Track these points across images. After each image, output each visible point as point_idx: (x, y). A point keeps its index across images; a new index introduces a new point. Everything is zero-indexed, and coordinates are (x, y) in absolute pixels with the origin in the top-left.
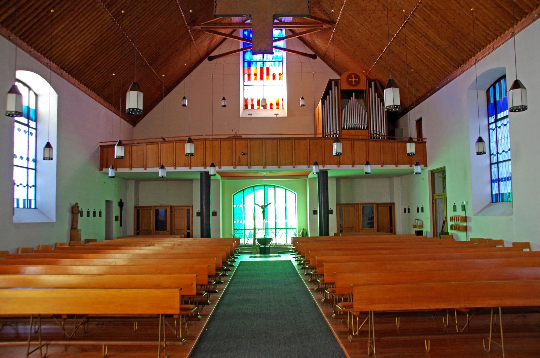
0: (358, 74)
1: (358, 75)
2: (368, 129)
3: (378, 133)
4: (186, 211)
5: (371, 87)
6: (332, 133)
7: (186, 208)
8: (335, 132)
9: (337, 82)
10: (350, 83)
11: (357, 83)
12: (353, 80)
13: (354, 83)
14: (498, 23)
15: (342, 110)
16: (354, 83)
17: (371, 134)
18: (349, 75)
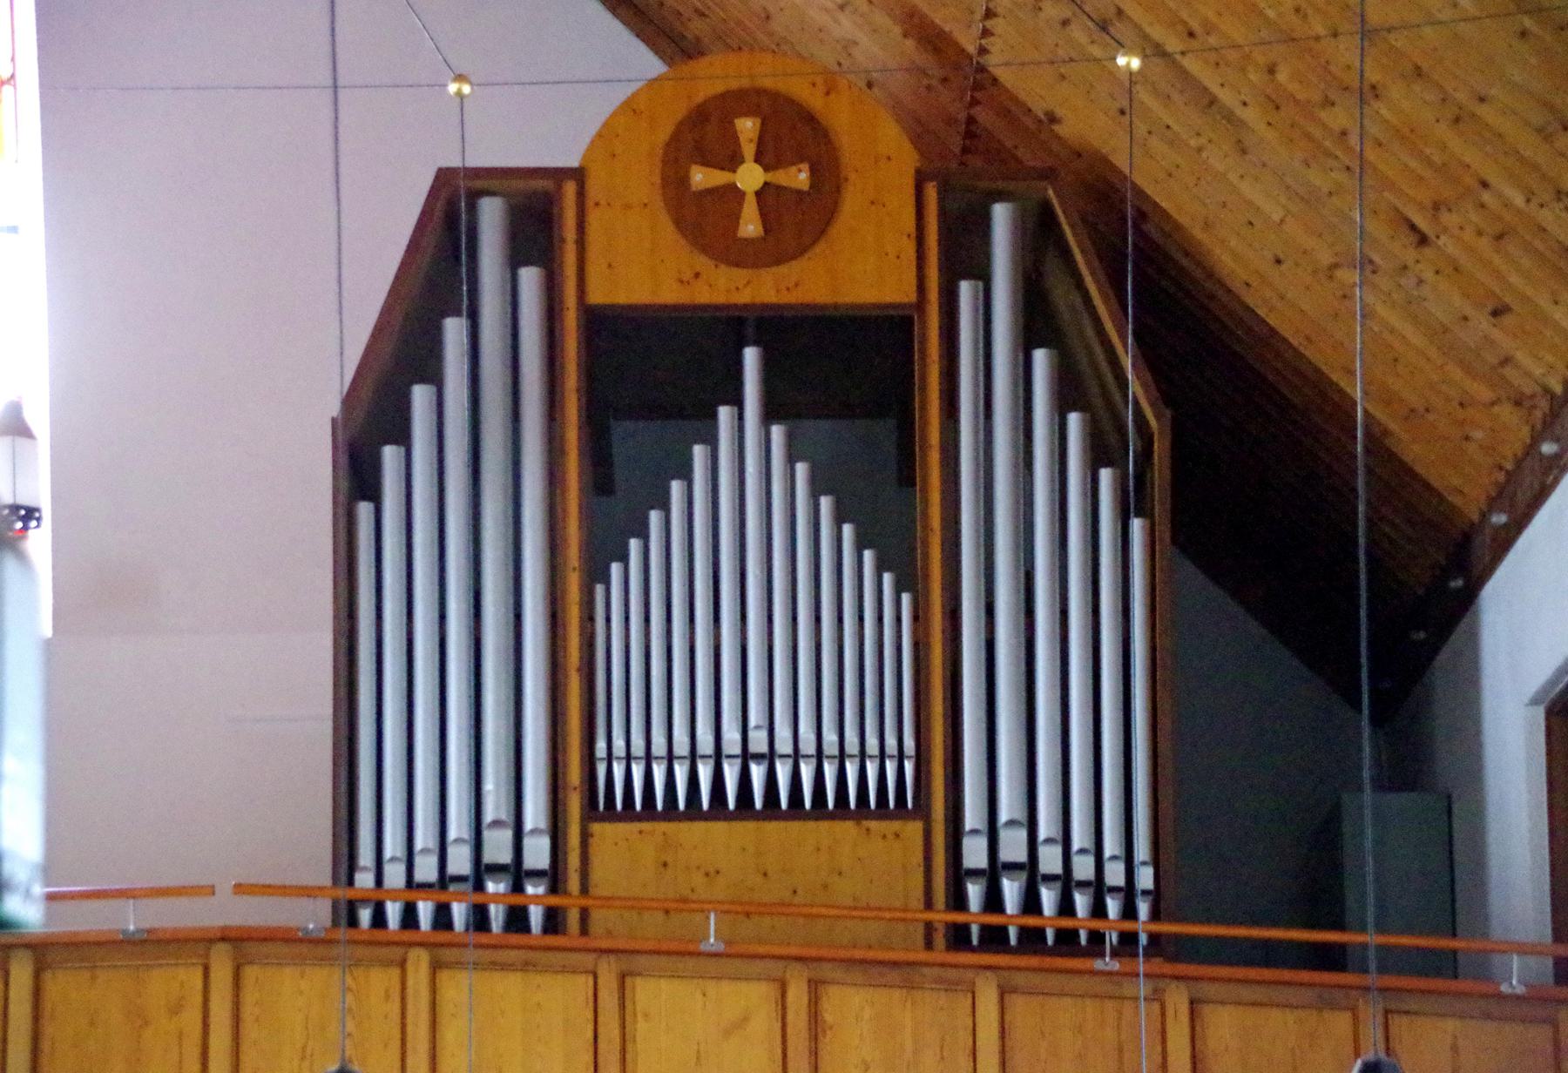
0: (814, 100)
1: (810, 118)
4: (620, 475)
5: (983, 275)
6: (395, 876)
8: (498, 848)
9: (541, 213)
10: (703, 222)
11: (800, 221)
12: (750, 177)
14: (1517, 78)
15: (596, 574)
16: (750, 226)
17: (958, 875)
18: (700, 116)
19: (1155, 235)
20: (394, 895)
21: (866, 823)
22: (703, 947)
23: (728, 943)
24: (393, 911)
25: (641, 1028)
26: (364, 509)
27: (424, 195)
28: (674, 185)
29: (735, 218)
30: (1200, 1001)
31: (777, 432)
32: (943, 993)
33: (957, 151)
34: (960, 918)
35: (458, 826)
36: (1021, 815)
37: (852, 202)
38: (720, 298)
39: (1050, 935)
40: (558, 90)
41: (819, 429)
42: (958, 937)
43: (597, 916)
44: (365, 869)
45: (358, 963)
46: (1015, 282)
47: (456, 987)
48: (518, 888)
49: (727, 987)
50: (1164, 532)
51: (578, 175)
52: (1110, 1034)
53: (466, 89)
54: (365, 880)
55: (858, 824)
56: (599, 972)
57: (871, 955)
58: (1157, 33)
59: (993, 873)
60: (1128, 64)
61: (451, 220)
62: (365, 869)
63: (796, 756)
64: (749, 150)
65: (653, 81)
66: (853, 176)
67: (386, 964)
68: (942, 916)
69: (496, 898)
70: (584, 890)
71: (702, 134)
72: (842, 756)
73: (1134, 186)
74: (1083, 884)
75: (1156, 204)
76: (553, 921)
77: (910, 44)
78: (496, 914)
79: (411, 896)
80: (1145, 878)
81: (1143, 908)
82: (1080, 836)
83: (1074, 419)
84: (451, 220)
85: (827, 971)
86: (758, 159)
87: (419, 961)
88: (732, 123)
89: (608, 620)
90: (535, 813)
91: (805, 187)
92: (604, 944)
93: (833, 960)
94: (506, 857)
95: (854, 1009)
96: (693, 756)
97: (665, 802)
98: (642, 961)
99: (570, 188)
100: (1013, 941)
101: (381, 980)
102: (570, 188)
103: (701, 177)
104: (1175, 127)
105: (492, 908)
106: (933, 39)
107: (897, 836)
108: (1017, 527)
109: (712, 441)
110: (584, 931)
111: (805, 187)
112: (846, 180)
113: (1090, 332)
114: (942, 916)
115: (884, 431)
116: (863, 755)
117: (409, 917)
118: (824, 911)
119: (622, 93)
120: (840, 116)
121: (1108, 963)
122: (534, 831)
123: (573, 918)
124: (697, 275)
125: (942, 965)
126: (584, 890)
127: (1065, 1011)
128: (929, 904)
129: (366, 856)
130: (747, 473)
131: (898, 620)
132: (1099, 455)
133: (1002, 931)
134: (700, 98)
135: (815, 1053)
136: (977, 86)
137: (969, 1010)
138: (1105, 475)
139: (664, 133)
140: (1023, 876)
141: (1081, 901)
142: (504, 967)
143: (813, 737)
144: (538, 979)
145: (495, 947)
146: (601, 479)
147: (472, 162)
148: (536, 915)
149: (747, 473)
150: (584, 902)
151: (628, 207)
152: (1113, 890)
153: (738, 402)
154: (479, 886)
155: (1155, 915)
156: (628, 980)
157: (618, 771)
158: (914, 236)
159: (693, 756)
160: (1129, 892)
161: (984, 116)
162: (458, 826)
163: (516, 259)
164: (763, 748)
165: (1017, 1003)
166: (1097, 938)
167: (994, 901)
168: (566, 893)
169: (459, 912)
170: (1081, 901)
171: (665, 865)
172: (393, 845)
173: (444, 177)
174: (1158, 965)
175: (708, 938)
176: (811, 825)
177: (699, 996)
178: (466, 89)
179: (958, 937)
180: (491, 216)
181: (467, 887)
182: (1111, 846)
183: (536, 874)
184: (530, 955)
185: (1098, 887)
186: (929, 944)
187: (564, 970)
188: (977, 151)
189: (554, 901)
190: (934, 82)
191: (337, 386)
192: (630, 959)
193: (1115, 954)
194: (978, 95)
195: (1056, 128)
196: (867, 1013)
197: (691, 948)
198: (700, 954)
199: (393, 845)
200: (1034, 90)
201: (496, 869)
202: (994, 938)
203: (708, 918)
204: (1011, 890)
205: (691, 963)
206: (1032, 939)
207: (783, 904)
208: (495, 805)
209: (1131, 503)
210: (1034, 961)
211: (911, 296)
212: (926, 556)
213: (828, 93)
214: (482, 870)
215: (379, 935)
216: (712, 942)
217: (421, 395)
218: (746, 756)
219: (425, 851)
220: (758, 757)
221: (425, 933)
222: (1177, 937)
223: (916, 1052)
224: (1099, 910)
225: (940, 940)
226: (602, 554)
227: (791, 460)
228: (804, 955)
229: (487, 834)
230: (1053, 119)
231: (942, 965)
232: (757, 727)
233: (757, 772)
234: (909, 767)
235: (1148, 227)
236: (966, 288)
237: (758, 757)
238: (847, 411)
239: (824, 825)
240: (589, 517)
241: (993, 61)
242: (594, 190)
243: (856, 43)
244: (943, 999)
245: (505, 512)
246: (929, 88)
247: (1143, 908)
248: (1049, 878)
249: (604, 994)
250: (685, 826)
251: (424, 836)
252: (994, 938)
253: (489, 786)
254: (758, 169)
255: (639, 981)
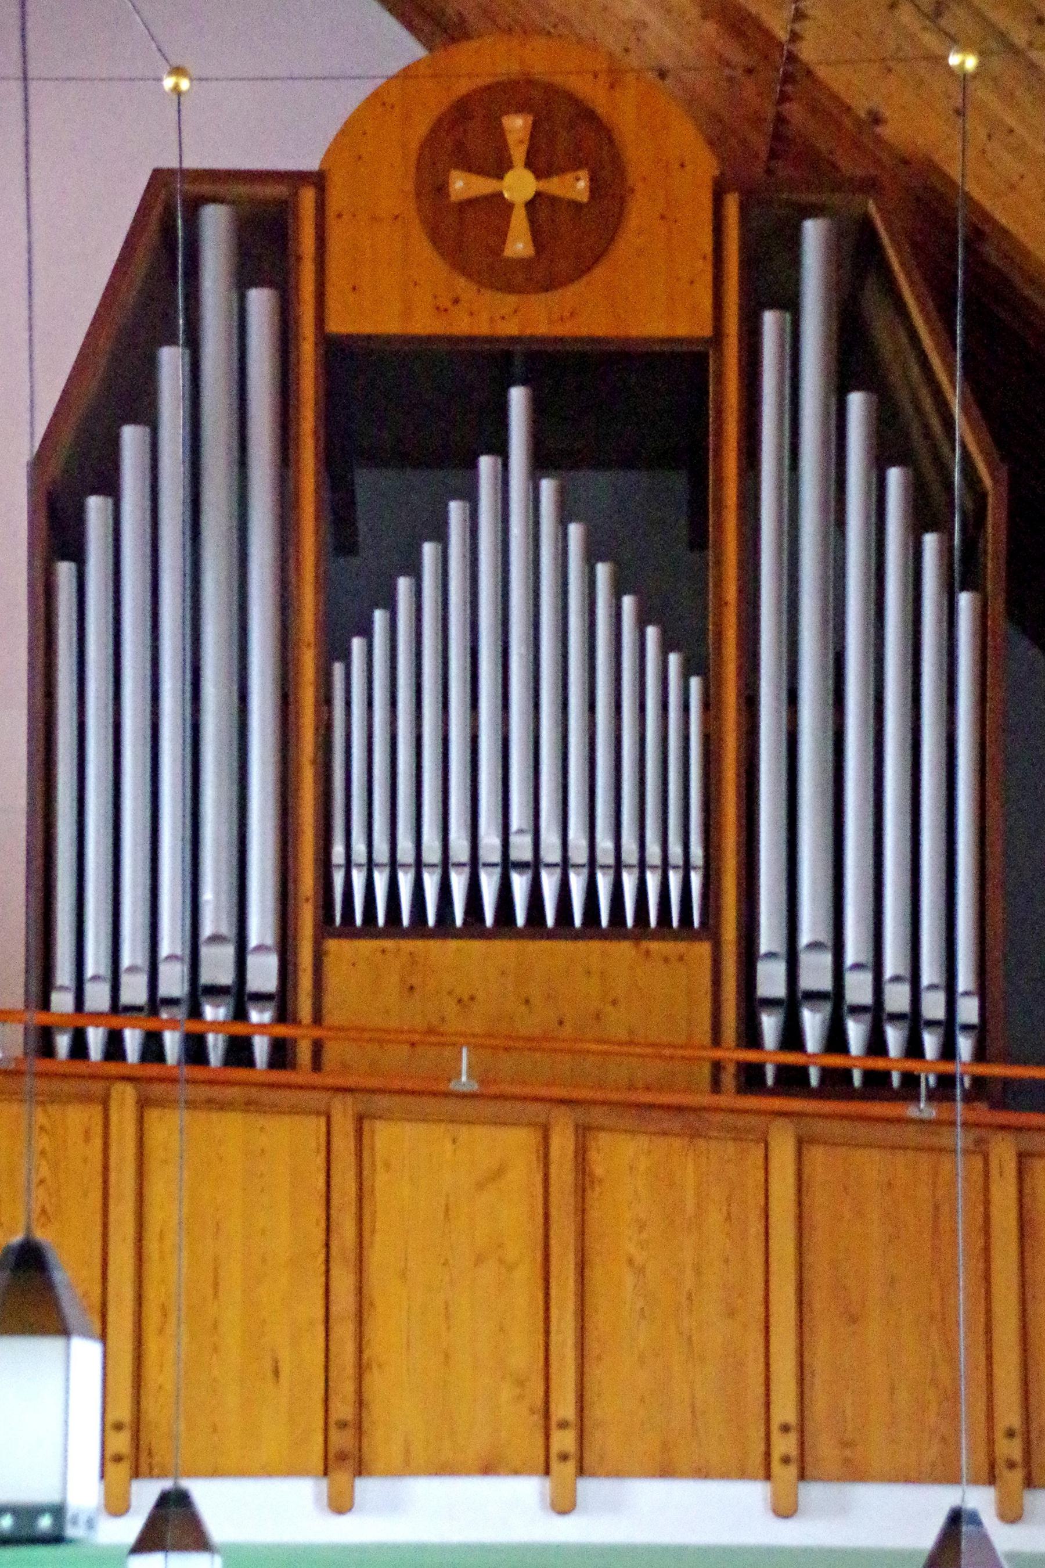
0: (593, 92)
1: (586, 115)
2: (711, 929)
3: (858, 989)
5: (790, 303)
6: (98, 997)
7: (110, 1432)
8: (217, 968)
9: (273, 224)
10: (463, 236)
11: (574, 241)
12: (519, 185)
13: (577, 186)
17: (751, 1005)
18: (460, 112)
19: (994, 259)
20: (96, 1017)
21: (645, 944)
22: (453, 1086)
23: (482, 1082)
24: (96, 1038)
25: (380, 1180)
26: (65, 570)
27: (142, 192)
28: (432, 190)
29: (502, 234)
30: (1031, 1155)
31: (547, 487)
32: (730, 1143)
33: (764, 155)
34: (751, 1056)
35: (171, 940)
36: (825, 936)
37: (640, 213)
38: (482, 328)
39: (814, 1077)
40: (296, 81)
41: (600, 484)
42: (751, 1078)
43: (332, 1052)
44: (62, 988)
45: (54, 1098)
46: (828, 309)
47: (166, 1128)
48: (240, 1014)
49: (480, 1132)
50: (998, 606)
51: (318, 180)
52: (924, 1192)
53: (185, 84)
54: (62, 1002)
55: (637, 945)
56: (333, 1112)
57: (647, 1098)
58: (1001, 18)
59: (791, 1005)
60: (963, 63)
61: (168, 230)
62: (62, 988)
63: (565, 865)
64: (518, 153)
65: (407, 74)
66: (640, 186)
67: (85, 1099)
68: (733, 1054)
69: (261, 1027)
70: (318, 1018)
71: (463, 133)
72: (618, 866)
73: (968, 198)
74: (895, 1017)
75: (995, 223)
76: (281, 1054)
77: (710, 28)
78: (215, 1045)
79: (116, 1022)
80: (968, 1010)
81: (965, 1045)
82: (893, 963)
83: (895, 476)
84: (168, 230)
85: (597, 1115)
86: (529, 164)
87: (124, 1096)
88: (498, 119)
89: (348, 704)
90: (261, 927)
91: (584, 198)
92: (340, 1082)
93: (603, 1103)
94: (226, 977)
95: (625, 1157)
96: (445, 864)
97: (412, 912)
98: (384, 1102)
99: (308, 196)
100: (770, 1081)
101: (79, 1117)
102: (308, 196)
103: (462, 185)
104: (1020, 130)
105: (211, 1038)
106: (740, 26)
107: (681, 958)
108: (906, 563)
109: (471, 497)
110: (317, 1064)
111: (584, 198)
112: (632, 191)
113: (915, 371)
114: (733, 1054)
115: (678, 481)
116: (643, 865)
117: (114, 1047)
118: (594, 1047)
119: (367, 89)
120: (623, 112)
121: (924, 1109)
122: (260, 948)
123: (304, 1053)
124: (456, 301)
125: (732, 1111)
126: (318, 1018)
127: (871, 1165)
128: (716, 1040)
129: (64, 974)
130: (513, 529)
131: (686, 708)
132: (924, 516)
133: (885, 1076)
134: (463, 87)
135: (582, 1212)
136: (788, 78)
137: (760, 1162)
138: (930, 540)
139: (421, 127)
140: (827, 1007)
141: (894, 1037)
142: (223, 1106)
143: (584, 843)
144: (262, 1121)
145: (211, 1082)
146: (342, 533)
147: (191, 162)
148: (261, 1046)
149: (513, 529)
150: (317, 1033)
151: (374, 219)
152: (932, 1024)
153: (501, 451)
154: (196, 1013)
155: (980, 1054)
156: (366, 1124)
157: (358, 879)
158: (710, 257)
159: (445, 864)
160: (949, 1027)
161: (795, 111)
162: (171, 940)
163: (245, 275)
164: (527, 856)
165: (817, 1154)
166: (911, 1080)
167: (792, 1036)
168: (296, 1022)
169: (172, 1042)
170: (894, 1037)
171: (412, 988)
172: (95, 962)
173: (160, 178)
174: (982, 1111)
175: (459, 1074)
176: (581, 945)
177: (448, 1145)
178: (185, 84)
179: (751, 1078)
180: (215, 224)
181: (180, 1013)
182: (930, 974)
183: (260, 997)
184: (254, 1092)
185: (914, 1021)
186: (716, 1086)
187: (294, 1110)
188: (787, 157)
189: (282, 1030)
190: (739, 73)
191: (27, 446)
192: (373, 1099)
193: (931, 1096)
194: (789, 88)
195: (879, 130)
196: (643, 1164)
197: (442, 1087)
198: (447, 1095)
199: (95, 962)
200: (856, 86)
201: (215, 991)
202: (792, 1079)
203: (460, 1052)
204: (813, 1023)
205: (430, 1104)
206: (836, 1081)
207: (546, 1038)
208: (214, 919)
209: (963, 573)
210: (796, 1105)
211: (706, 330)
212: (719, 635)
213: (612, 86)
214: (199, 993)
215: (79, 1067)
216: (464, 1082)
217: (131, 436)
218: (507, 865)
219: (132, 969)
220: (521, 866)
221: (132, 1066)
222: (1007, 1083)
223: (699, 1206)
224: (914, 1048)
225: (728, 1078)
226: (342, 627)
227: (563, 521)
228: (563, 1094)
229: (205, 951)
230: (876, 119)
231: (732, 1111)
232: (521, 831)
233: (520, 883)
234: (696, 880)
235: (990, 251)
236: (770, 319)
237: (521, 866)
238: (627, 462)
239: (596, 946)
240: (325, 584)
241: (807, 52)
242: (337, 198)
243: (645, 25)
244: (731, 1147)
245: (229, 578)
246: (731, 80)
247: (965, 1045)
248: (857, 1010)
249: (337, 1143)
250: (434, 946)
251: (132, 953)
252: (792, 1079)
253: (207, 895)
254: (528, 177)
255: (379, 1124)
